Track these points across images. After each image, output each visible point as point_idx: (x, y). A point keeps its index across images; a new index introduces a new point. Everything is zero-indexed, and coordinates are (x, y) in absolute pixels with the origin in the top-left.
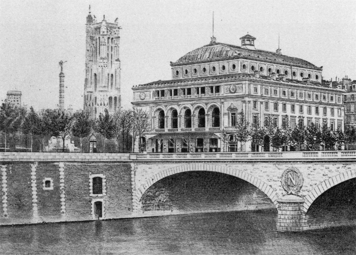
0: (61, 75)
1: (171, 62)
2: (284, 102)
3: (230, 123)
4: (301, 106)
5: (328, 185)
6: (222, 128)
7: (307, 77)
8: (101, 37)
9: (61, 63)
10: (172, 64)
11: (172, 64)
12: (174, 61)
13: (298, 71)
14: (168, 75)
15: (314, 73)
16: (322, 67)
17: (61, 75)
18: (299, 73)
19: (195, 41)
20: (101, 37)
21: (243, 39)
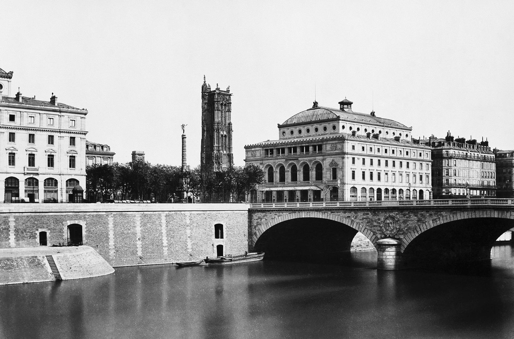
0: (183, 137)
1: (278, 124)
2: (421, 162)
3: (332, 177)
4: (421, 164)
5: (287, 217)
6: (324, 180)
7: (378, 132)
8: (214, 103)
9: (183, 126)
10: (280, 127)
11: (280, 127)
12: (281, 124)
13: (391, 131)
14: (274, 136)
15: (404, 133)
16: (12, 73)
17: (183, 137)
18: (389, 134)
19: (297, 107)
20: (214, 103)
21: (342, 103)
